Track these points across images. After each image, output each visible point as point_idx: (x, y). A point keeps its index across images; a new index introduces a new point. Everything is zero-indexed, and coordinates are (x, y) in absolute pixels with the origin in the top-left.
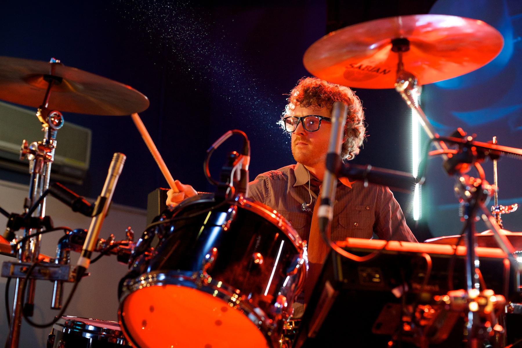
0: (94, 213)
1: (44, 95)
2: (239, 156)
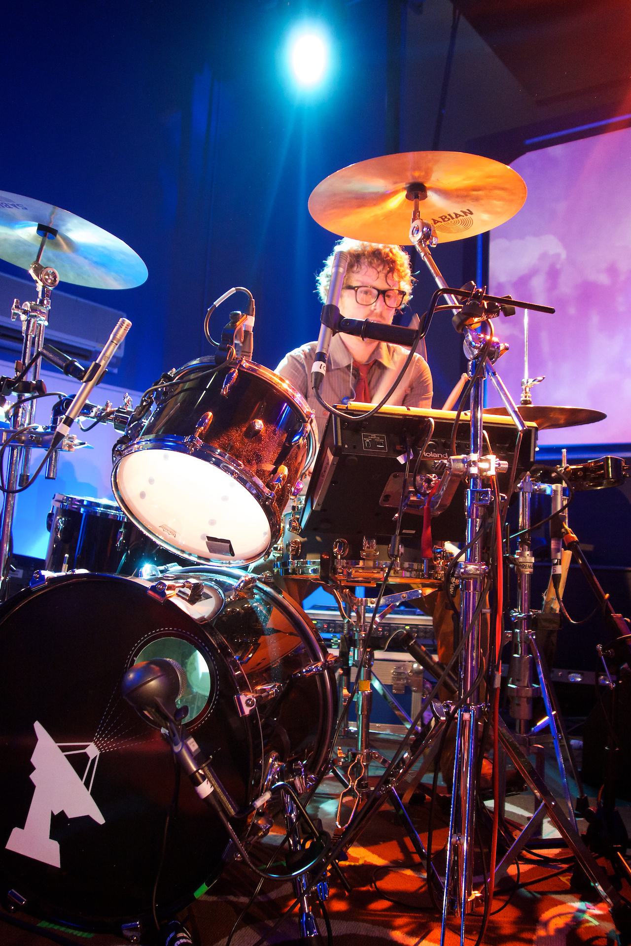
0: (85, 379)
1: (39, 246)
2: (243, 316)
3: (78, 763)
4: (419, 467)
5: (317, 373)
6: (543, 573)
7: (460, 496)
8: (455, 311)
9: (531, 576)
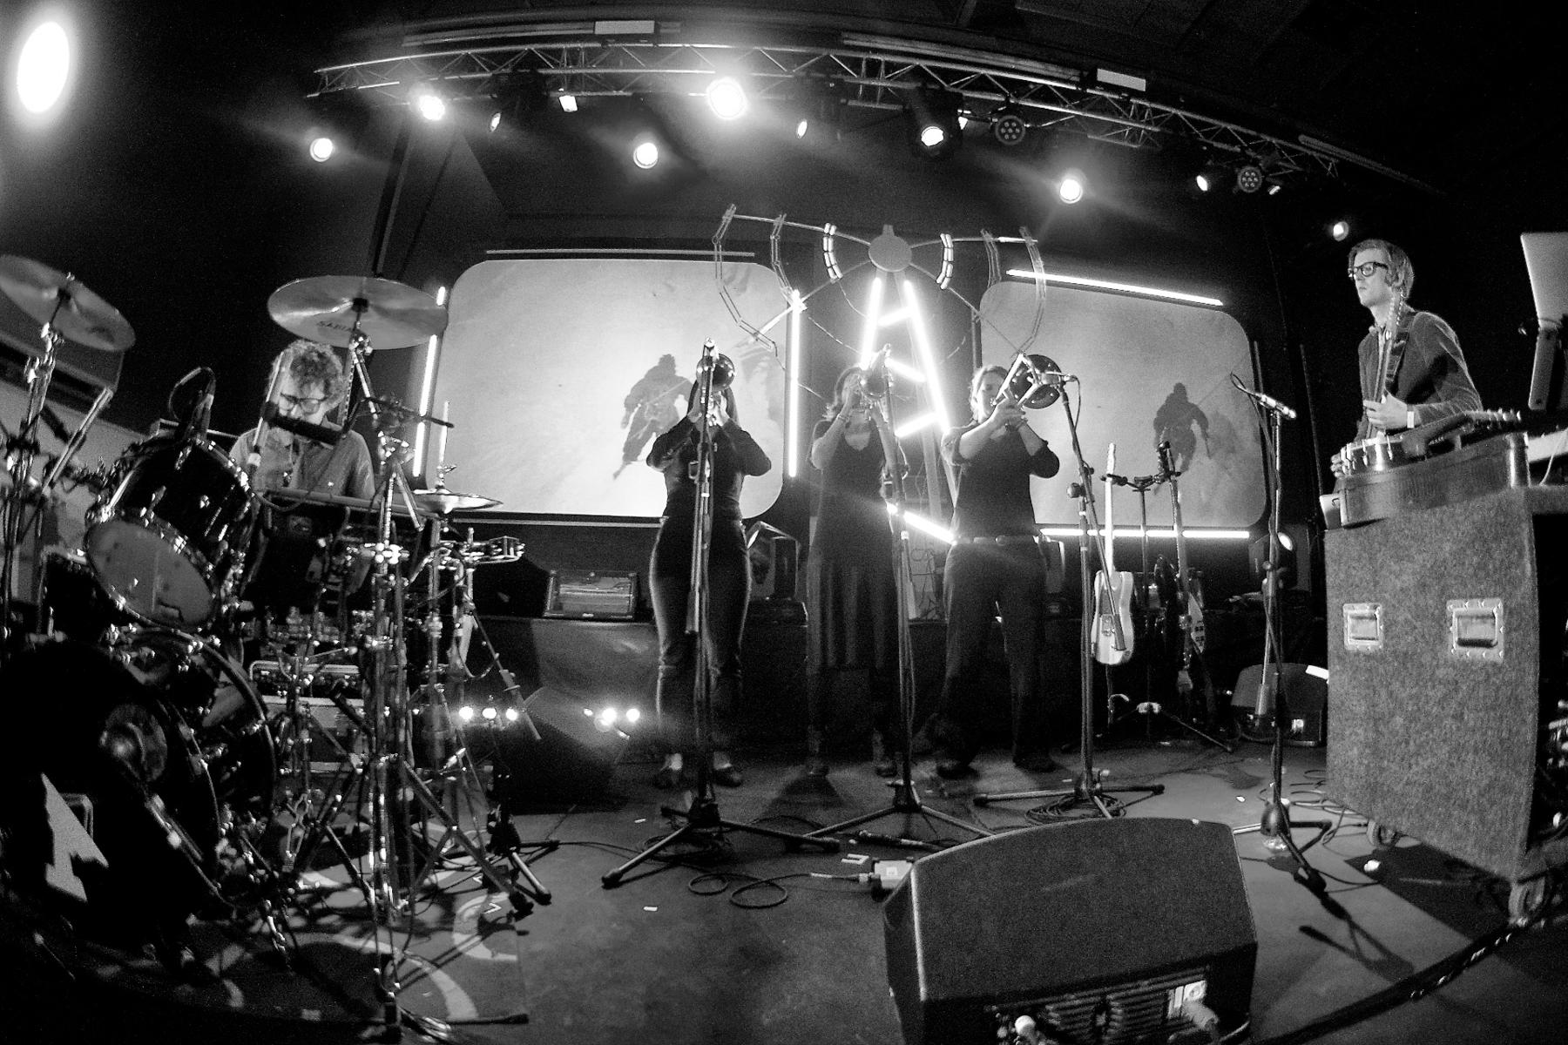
3: (79, 812)
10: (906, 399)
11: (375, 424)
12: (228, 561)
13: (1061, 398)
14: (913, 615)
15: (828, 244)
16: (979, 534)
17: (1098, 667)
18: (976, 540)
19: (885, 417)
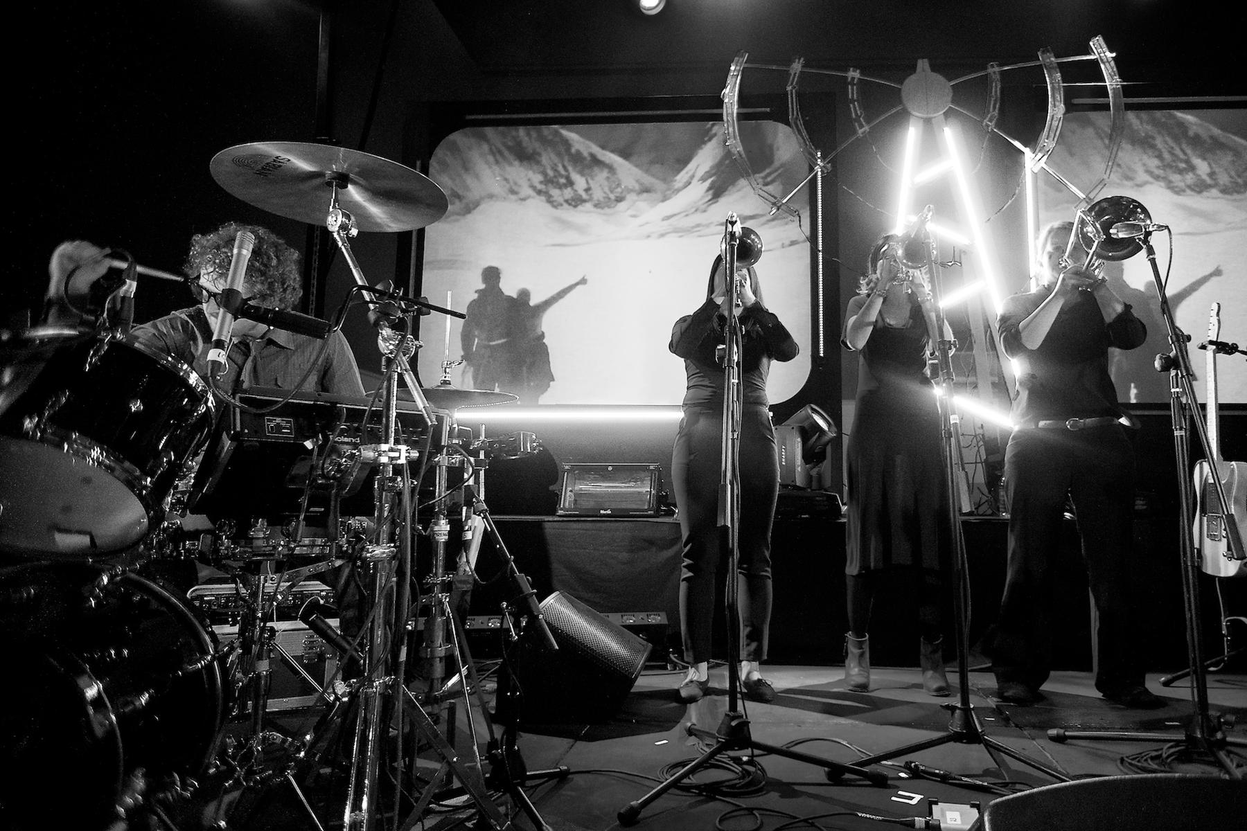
4: (327, 449)
5: (214, 362)
6: (457, 543)
7: (369, 481)
8: (371, 306)
9: (447, 544)
10: (950, 265)
11: (372, 317)
12: (176, 470)
13: (1143, 253)
14: (966, 508)
15: (853, 92)
16: (1046, 418)
17: (1207, 581)
18: (1042, 424)
19: (927, 288)
